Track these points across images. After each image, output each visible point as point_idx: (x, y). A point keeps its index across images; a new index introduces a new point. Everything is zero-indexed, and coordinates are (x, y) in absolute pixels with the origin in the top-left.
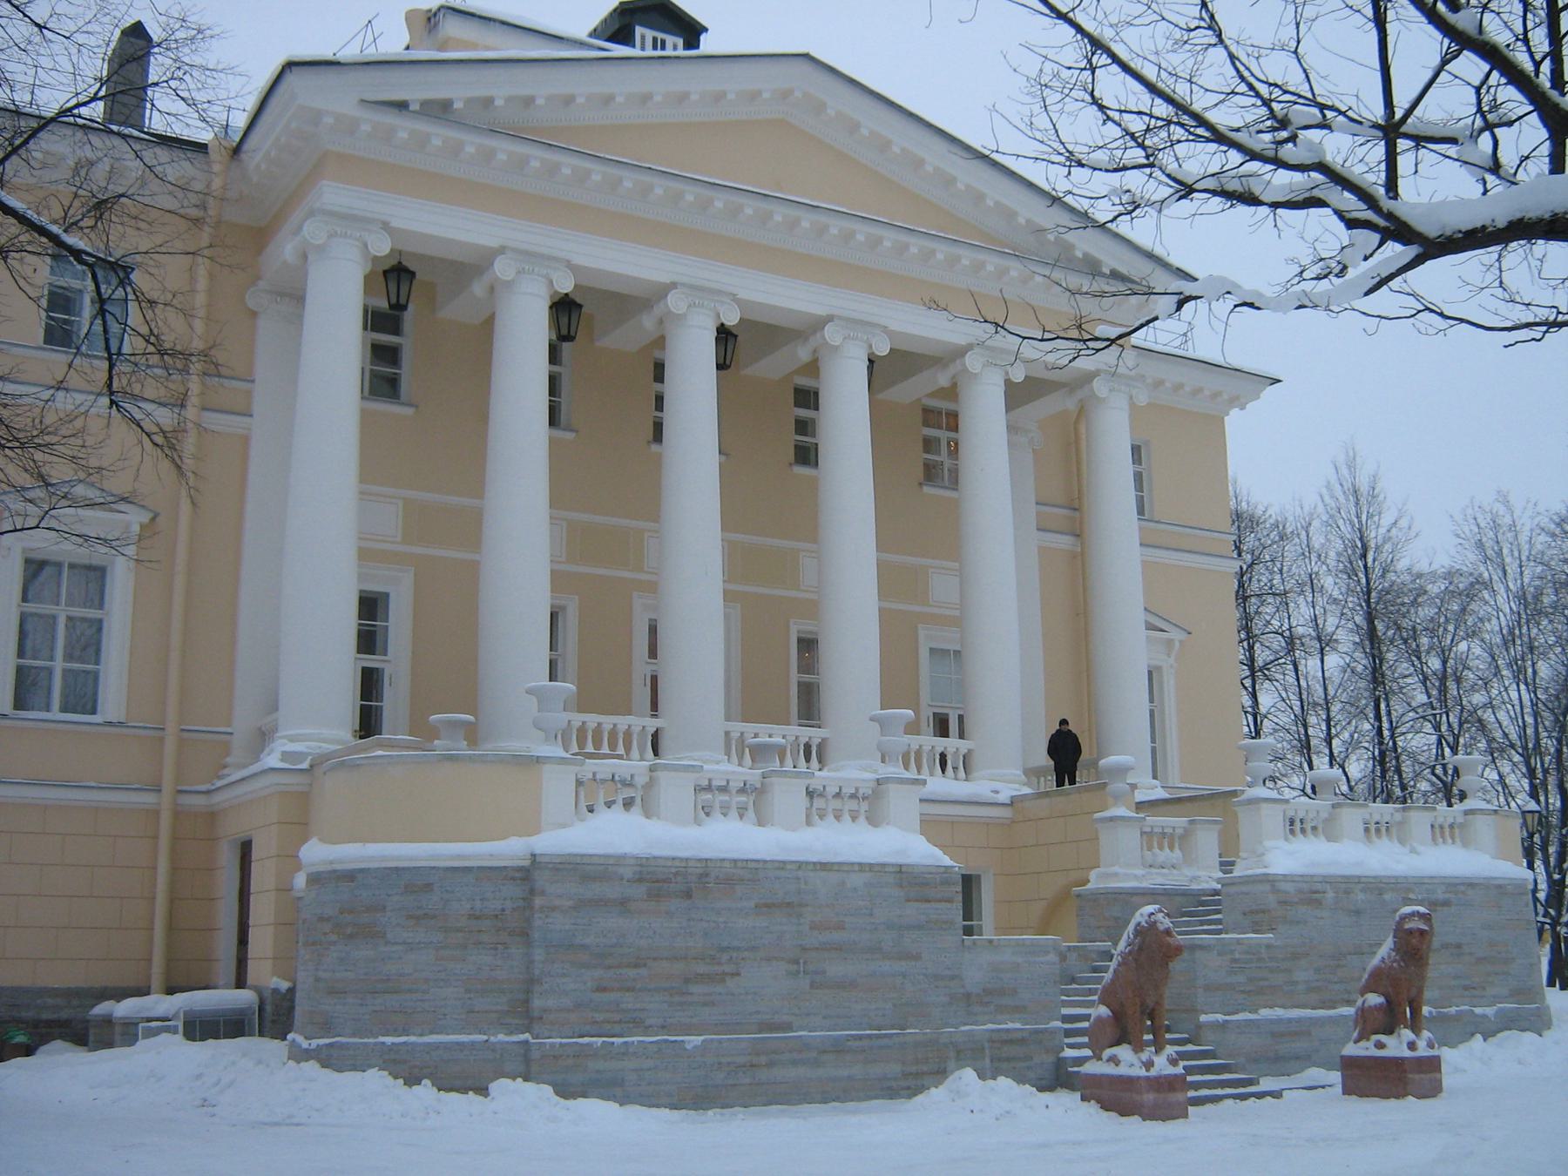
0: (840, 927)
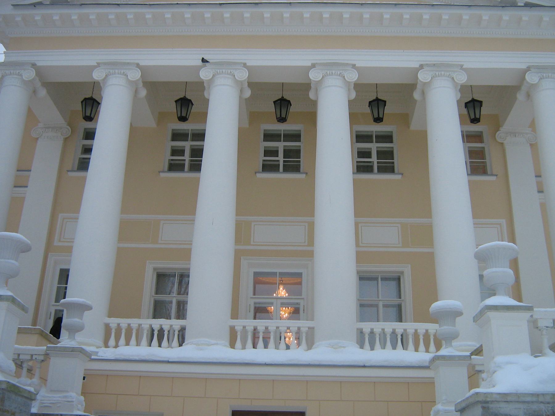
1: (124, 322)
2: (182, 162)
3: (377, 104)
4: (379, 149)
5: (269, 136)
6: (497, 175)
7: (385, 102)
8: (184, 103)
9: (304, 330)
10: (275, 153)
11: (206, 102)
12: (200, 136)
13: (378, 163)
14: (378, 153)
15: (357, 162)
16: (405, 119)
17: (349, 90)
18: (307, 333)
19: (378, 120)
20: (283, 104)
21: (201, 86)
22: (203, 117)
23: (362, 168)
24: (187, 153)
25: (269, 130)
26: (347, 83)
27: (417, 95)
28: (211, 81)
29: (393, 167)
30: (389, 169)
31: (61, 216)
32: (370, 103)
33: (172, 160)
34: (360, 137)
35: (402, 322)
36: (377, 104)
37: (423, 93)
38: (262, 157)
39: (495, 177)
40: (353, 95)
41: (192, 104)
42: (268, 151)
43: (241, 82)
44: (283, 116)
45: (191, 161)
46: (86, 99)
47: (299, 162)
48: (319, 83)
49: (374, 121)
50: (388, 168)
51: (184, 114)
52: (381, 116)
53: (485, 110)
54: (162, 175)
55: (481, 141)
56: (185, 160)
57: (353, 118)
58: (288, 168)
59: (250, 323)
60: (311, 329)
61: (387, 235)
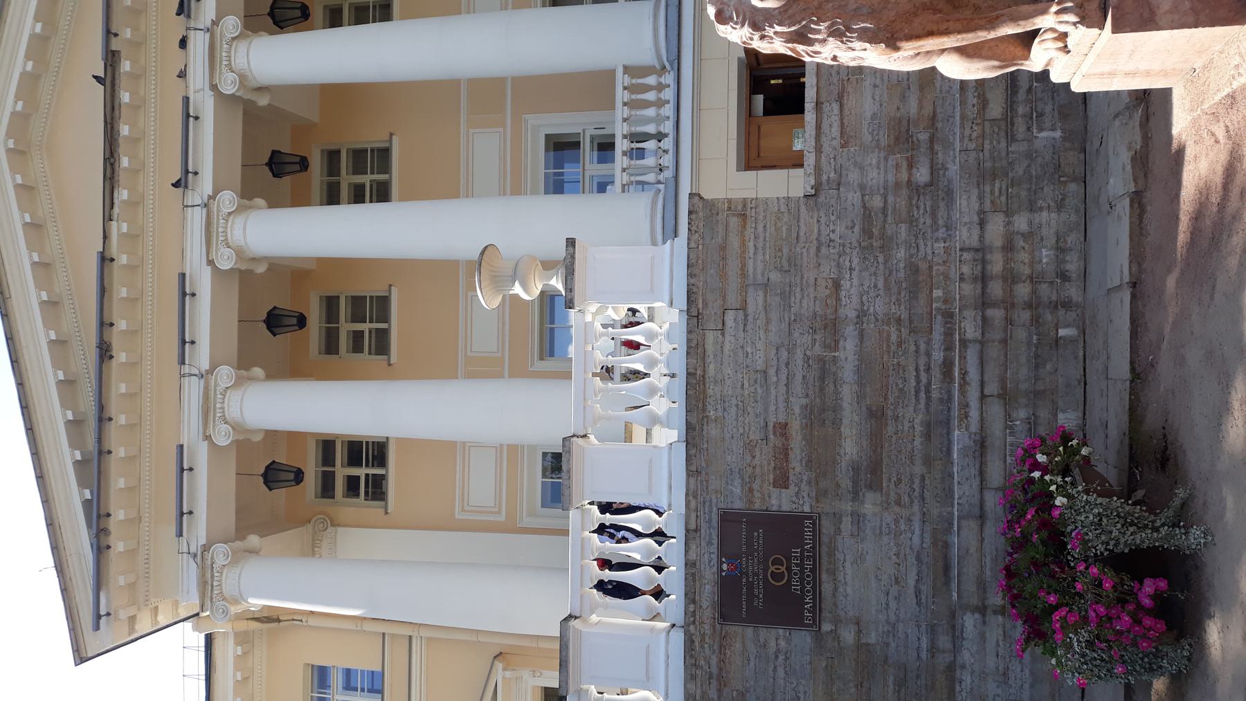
0: (783, 429)
1: (621, 95)
2: (375, 187)
3: (274, 321)
4: (351, 169)
5: (331, 346)
6: (391, 134)
7: (274, 152)
8: (273, 476)
9: (627, 80)
10: (357, 337)
11: (272, 435)
12: (327, 446)
13: (372, 173)
14: (355, 172)
15: (370, 353)
16: (302, 129)
17: (250, 379)
18: (632, 93)
19: (302, 321)
20: (274, 321)
21: (244, 445)
22: (294, 438)
23: (382, 194)
24: (354, 471)
25: (321, 190)
26: (240, 209)
27: (263, 101)
28: (237, 427)
29: (379, 150)
30: (383, 303)
31: (459, 516)
32: (275, 176)
33: (366, 493)
34: (332, 198)
35: (614, 144)
36: (278, 164)
37: (260, 89)
38: (365, 356)
39: (394, 137)
40: (260, 201)
41: (275, 308)
42: (355, 196)
43: (234, 552)
44: (298, 159)
45: (367, 465)
46: (266, 483)
47: (371, 297)
48: (240, 253)
49: (298, 483)
50: (383, 156)
51: (294, 321)
52: (298, 159)
53: (285, 303)
54: (393, 360)
55: (339, 152)
56: (367, 475)
57: (299, 200)
58: (384, 316)
59: (620, 161)
60: (627, 69)
61: (485, 148)
